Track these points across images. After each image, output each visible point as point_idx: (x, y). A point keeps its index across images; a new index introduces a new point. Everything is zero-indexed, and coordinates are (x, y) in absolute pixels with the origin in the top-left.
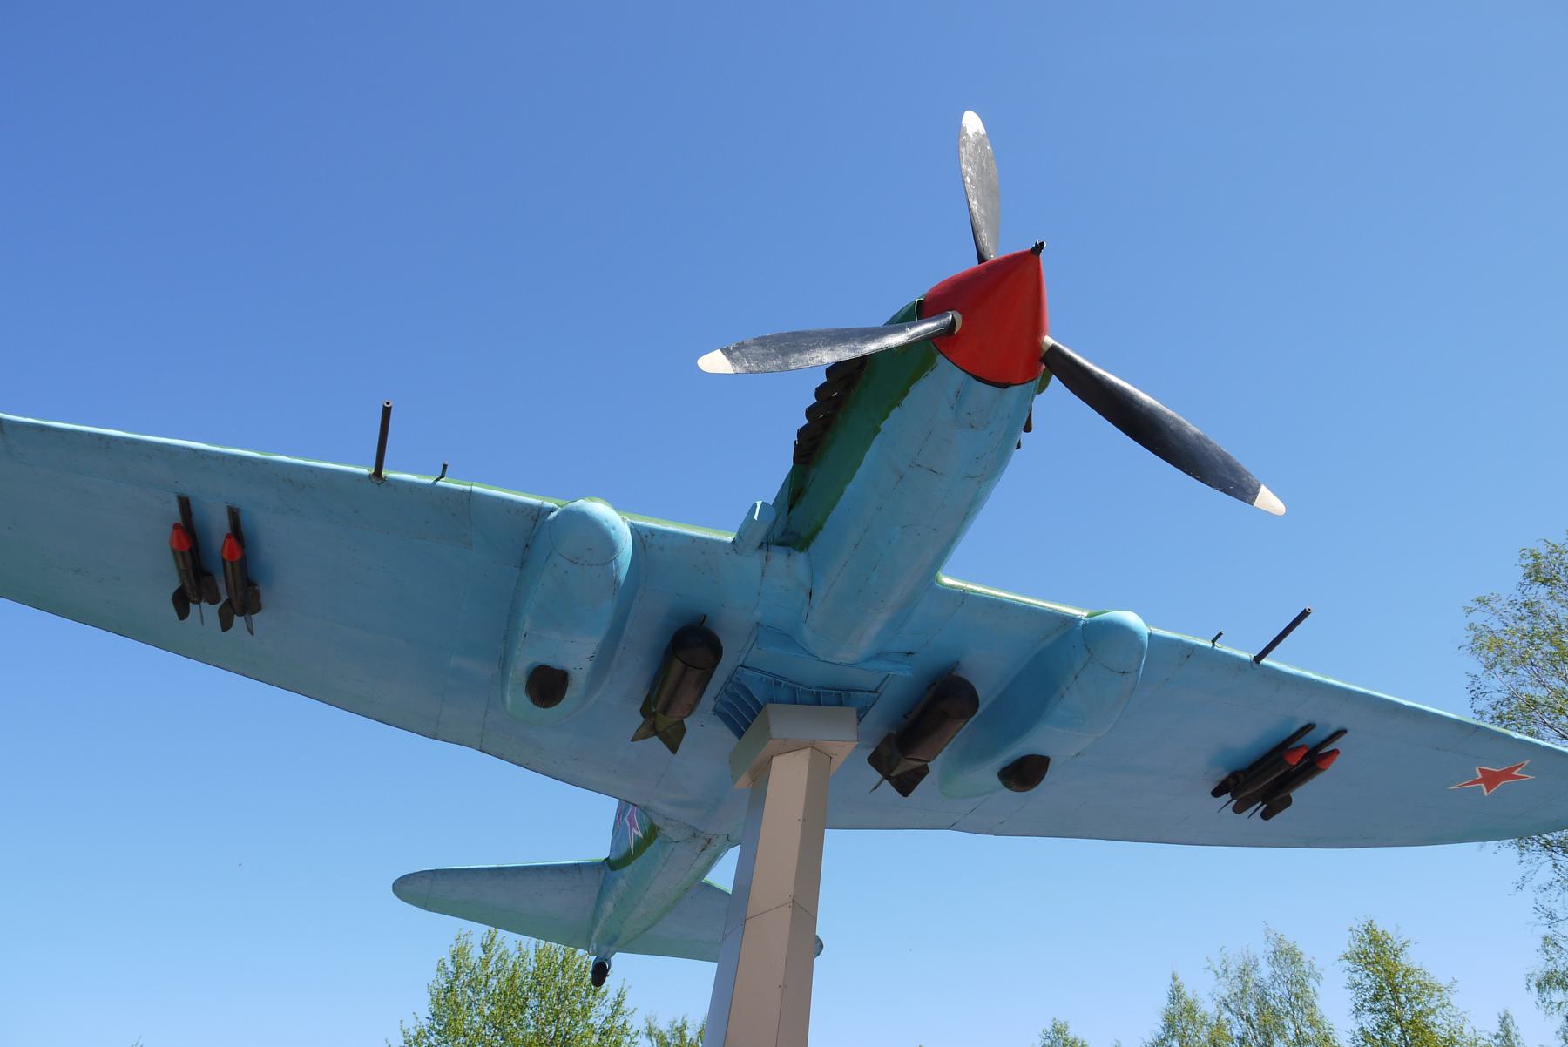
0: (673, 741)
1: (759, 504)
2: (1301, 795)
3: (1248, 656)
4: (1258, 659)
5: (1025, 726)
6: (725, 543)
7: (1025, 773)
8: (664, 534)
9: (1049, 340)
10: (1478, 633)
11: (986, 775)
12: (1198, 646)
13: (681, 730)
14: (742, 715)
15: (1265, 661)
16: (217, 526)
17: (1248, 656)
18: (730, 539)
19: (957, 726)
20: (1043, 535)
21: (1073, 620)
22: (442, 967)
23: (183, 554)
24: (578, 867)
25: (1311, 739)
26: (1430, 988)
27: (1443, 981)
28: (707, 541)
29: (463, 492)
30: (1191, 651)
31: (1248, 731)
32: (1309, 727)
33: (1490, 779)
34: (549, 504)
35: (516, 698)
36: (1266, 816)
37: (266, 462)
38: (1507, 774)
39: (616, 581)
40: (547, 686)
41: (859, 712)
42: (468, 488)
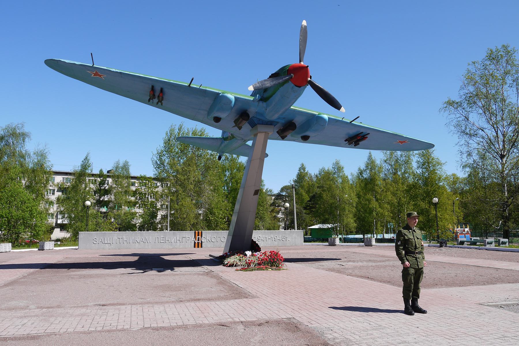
0: (240, 128)
3: (349, 121)
4: (351, 122)
5: (306, 130)
10: (469, 71)
11: (300, 136)
13: (242, 128)
14: (253, 125)
22: (167, 134)
24: (217, 138)
25: (362, 135)
26: (439, 164)
27: (443, 162)
31: (353, 132)
32: (362, 133)
33: (401, 142)
34: (220, 92)
38: (404, 142)
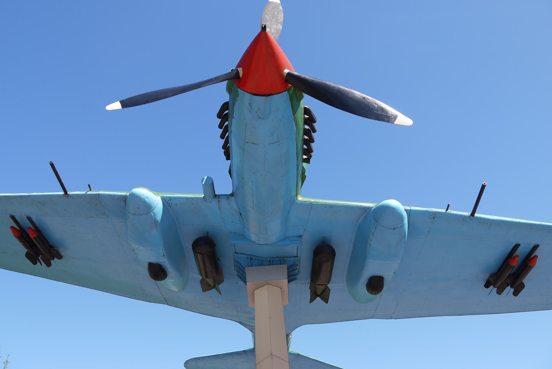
1: (205, 178)
2: (529, 280)
3: (468, 214)
4: (473, 214)
6: (200, 198)
7: (375, 285)
8: (175, 198)
9: (286, 71)
12: (437, 212)
15: (476, 215)
16: (27, 224)
17: (468, 214)
18: (203, 196)
19: (330, 266)
20: (343, 177)
21: (369, 208)
23: (18, 237)
25: (521, 252)
28: (193, 198)
29: (96, 194)
30: (434, 215)
31: (492, 254)
32: (517, 246)
35: (361, 288)
36: (516, 294)
37: (29, 196)
39: (155, 221)
40: (375, 285)
41: (288, 268)
42: (98, 193)
